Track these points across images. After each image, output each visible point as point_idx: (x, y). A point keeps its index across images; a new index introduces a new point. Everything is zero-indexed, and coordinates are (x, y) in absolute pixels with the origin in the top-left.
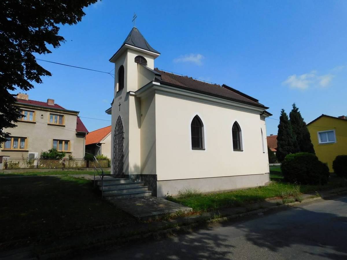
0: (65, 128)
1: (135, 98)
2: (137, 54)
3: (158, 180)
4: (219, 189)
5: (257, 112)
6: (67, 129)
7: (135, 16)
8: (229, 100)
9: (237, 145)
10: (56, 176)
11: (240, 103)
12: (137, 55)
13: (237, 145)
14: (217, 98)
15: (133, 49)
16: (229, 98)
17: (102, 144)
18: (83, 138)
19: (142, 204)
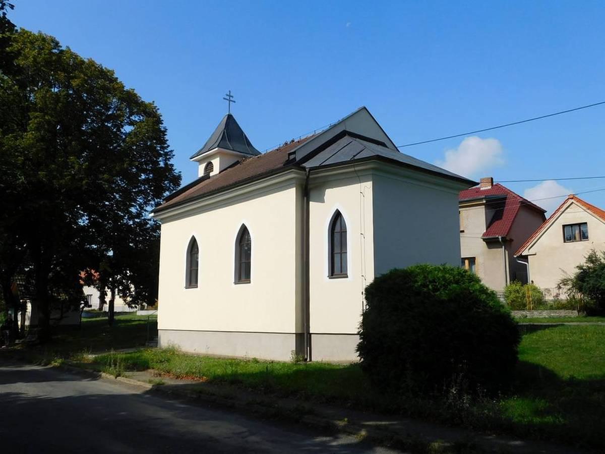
0: (465, 235)
1: (327, 188)
2: (205, 162)
3: (294, 335)
4: (179, 346)
5: (284, 184)
6: (468, 236)
7: (228, 98)
8: (216, 193)
9: (243, 272)
10: (148, 316)
11: (201, 200)
12: (206, 163)
13: (243, 272)
14: (179, 207)
15: (213, 153)
16: (258, 177)
17: (529, 257)
18: (502, 247)
19: (40, 328)
